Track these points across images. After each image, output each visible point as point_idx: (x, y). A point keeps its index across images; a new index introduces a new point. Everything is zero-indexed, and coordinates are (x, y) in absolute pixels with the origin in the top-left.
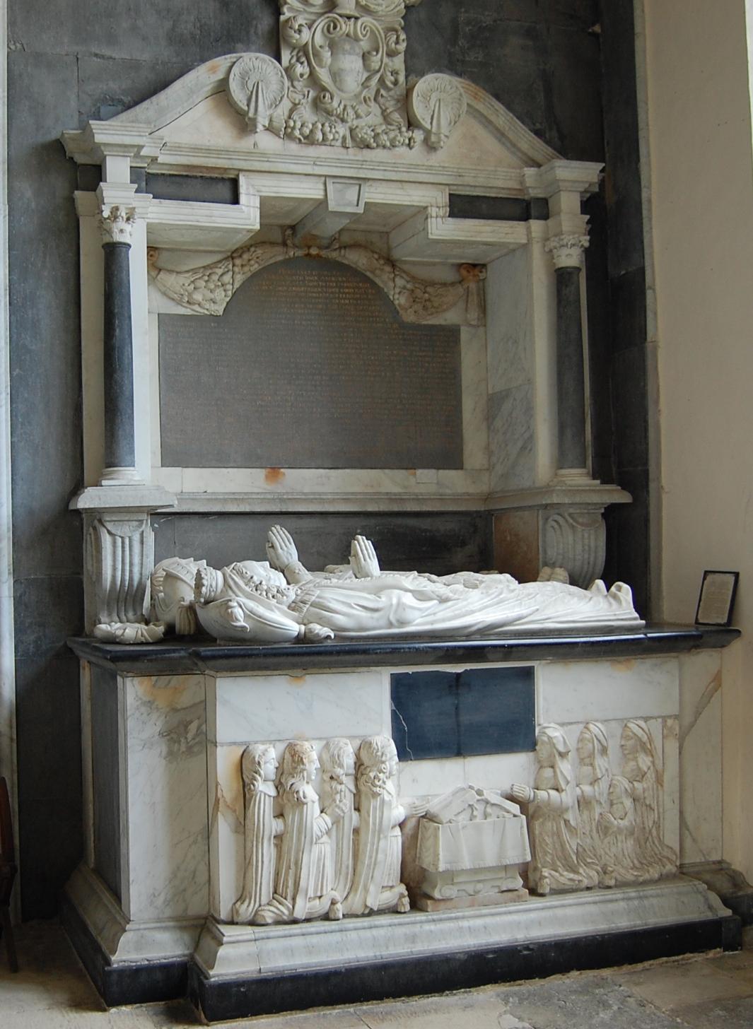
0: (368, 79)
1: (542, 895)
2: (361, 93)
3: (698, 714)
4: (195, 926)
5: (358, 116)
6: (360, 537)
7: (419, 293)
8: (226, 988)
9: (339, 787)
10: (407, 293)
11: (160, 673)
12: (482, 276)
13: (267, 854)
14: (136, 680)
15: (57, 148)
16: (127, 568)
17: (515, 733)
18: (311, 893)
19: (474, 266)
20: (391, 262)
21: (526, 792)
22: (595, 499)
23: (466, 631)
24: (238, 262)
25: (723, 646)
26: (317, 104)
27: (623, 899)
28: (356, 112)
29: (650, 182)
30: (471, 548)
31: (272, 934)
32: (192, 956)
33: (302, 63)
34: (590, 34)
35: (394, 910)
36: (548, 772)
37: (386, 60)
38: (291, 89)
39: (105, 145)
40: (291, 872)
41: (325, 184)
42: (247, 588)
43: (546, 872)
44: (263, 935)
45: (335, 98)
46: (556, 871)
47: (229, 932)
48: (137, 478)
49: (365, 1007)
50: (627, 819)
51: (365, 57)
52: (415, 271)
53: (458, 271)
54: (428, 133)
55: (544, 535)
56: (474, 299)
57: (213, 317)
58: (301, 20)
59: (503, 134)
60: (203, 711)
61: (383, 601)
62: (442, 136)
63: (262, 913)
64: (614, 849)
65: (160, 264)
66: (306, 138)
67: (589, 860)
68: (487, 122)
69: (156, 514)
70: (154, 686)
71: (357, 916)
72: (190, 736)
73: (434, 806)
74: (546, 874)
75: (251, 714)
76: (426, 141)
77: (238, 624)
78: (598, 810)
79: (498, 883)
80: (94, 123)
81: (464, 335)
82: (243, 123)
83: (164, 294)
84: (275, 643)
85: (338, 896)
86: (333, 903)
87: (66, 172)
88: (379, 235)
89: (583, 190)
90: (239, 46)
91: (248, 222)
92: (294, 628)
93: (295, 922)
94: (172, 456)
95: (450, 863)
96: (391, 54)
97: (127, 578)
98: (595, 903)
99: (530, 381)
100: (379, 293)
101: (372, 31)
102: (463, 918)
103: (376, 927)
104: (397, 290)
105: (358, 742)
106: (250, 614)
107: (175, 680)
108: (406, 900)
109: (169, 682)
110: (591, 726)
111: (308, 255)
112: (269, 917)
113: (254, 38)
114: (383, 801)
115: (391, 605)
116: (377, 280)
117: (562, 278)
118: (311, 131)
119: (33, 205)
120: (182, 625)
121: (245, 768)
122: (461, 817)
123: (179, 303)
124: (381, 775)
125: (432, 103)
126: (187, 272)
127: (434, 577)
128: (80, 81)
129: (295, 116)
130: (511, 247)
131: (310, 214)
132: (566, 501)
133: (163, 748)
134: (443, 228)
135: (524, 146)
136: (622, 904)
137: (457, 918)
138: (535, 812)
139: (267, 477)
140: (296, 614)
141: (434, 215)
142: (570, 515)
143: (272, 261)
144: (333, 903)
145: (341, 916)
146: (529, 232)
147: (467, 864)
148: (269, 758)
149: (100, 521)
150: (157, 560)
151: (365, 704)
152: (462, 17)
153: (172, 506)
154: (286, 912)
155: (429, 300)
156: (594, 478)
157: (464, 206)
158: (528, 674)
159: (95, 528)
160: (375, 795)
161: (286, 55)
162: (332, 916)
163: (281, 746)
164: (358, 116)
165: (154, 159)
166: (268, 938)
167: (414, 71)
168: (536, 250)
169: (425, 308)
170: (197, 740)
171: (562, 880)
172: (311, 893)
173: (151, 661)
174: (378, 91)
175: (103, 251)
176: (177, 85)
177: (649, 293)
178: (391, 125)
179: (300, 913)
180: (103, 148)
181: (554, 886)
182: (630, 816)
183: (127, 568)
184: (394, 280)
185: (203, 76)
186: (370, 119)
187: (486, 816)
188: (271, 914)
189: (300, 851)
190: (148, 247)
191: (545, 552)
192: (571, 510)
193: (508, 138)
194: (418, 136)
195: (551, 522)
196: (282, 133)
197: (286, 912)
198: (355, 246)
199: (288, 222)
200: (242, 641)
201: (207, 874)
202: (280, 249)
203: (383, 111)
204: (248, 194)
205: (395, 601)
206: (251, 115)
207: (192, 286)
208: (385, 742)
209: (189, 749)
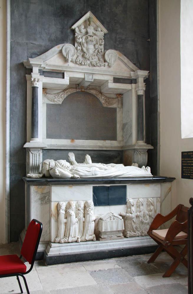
0: (95, 50)
1: (127, 238)
2: (93, 53)
3: (165, 197)
4: (46, 243)
5: (92, 59)
6: (87, 155)
7: (107, 100)
8: (51, 258)
9: (80, 212)
10: (104, 100)
11: (39, 185)
12: (122, 96)
13: (63, 227)
14: (34, 187)
15: (22, 64)
16: (36, 161)
17: (122, 200)
18: (73, 236)
19: (120, 94)
20: (101, 93)
21: (124, 214)
22: (145, 148)
23: (111, 177)
24: (65, 92)
25: (171, 182)
26: (83, 56)
27: (146, 239)
28: (92, 58)
29: (159, 76)
30: (118, 159)
31: (63, 245)
32: (45, 250)
33: (80, 46)
34: (147, 41)
35: (92, 240)
36: (129, 210)
37: (99, 46)
38: (77, 52)
39: (33, 64)
40: (68, 231)
41: (84, 74)
42: (60, 166)
43: (128, 232)
44: (61, 245)
45: (87, 55)
46: (131, 232)
47: (53, 245)
48: (39, 141)
49: (84, 262)
50: (147, 221)
51: (94, 45)
52: (106, 95)
53: (117, 96)
54: (109, 63)
55: (134, 156)
56: (120, 102)
57: (59, 105)
58: (79, 36)
59: (126, 64)
60: (49, 194)
61: (91, 169)
62: (112, 64)
63: (61, 240)
64: (144, 228)
65: (47, 92)
66: (80, 64)
67: (138, 230)
68: (123, 61)
69: (43, 149)
70: (38, 188)
71: (83, 242)
72: (46, 200)
73: (102, 217)
74: (128, 233)
75: (60, 195)
76: (108, 65)
77: (57, 174)
78: (141, 218)
79: (116, 235)
80: (30, 59)
81: (118, 110)
82: (66, 60)
83: (48, 99)
84: (66, 179)
85: (79, 237)
86: (78, 238)
87: (23, 71)
88: (98, 86)
89: (144, 77)
90: (65, 42)
91: (66, 83)
92: (70, 175)
93: (69, 243)
94: (49, 135)
95: (105, 230)
96: (101, 45)
97: (36, 163)
98: (139, 239)
99: (131, 121)
100: (98, 100)
101: (96, 40)
102: (108, 242)
103: (87, 244)
104: (102, 99)
105: (85, 202)
106: (60, 172)
107: (43, 187)
108: (95, 238)
109: (41, 187)
110: (140, 199)
111: (82, 91)
112: (63, 241)
113: (69, 40)
114: (90, 215)
115: (93, 171)
116: (98, 97)
117: (139, 97)
118: (81, 62)
119: (16, 78)
120: (46, 175)
121: (58, 207)
122: (108, 219)
123: (51, 101)
124: (90, 209)
125: (110, 56)
126: (53, 94)
127: (105, 164)
128: (28, 49)
129: (78, 59)
130: (128, 90)
131: (81, 82)
132: (138, 148)
133: (40, 202)
134: (112, 85)
135: (131, 67)
136: (146, 240)
137: (107, 242)
138: (126, 219)
139: (71, 141)
140: (71, 172)
141: (110, 82)
142: (140, 151)
143: (73, 92)
144: (78, 238)
145: (80, 241)
146: (132, 87)
147: (109, 230)
148: (64, 205)
149: (30, 151)
150: (44, 159)
151: (86, 193)
152: (118, 37)
153: (46, 147)
154: (67, 240)
155: (109, 102)
156: (146, 143)
157: (117, 80)
158: (125, 187)
159: (28, 152)
160: (88, 214)
161: (76, 45)
162: (77, 241)
163: (67, 202)
164: (92, 59)
165: (44, 68)
166: (62, 246)
167: (106, 49)
168: (133, 91)
169: (109, 104)
170: (48, 200)
171: (132, 234)
172: (73, 236)
173: (36, 182)
174: (97, 54)
175: (32, 89)
176: (50, 51)
177: (158, 101)
178: (100, 61)
179: (70, 241)
180: (32, 65)
181: (130, 236)
182: (148, 220)
183: (36, 161)
184: (101, 97)
185: (56, 49)
186: (95, 60)
187: (114, 219)
188: (63, 241)
189: (70, 226)
190: (43, 88)
191: (134, 160)
192: (140, 150)
193: (127, 65)
194: (106, 64)
195: (135, 153)
196: (75, 62)
197: (67, 240)
198: (93, 89)
199: (77, 83)
200: (58, 178)
201: (49, 232)
202: (75, 89)
203: (98, 58)
204: (66, 76)
205: (94, 170)
206: (67, 58)
207: (54, 98)
208: (91, 202)
209: (46, 202)
